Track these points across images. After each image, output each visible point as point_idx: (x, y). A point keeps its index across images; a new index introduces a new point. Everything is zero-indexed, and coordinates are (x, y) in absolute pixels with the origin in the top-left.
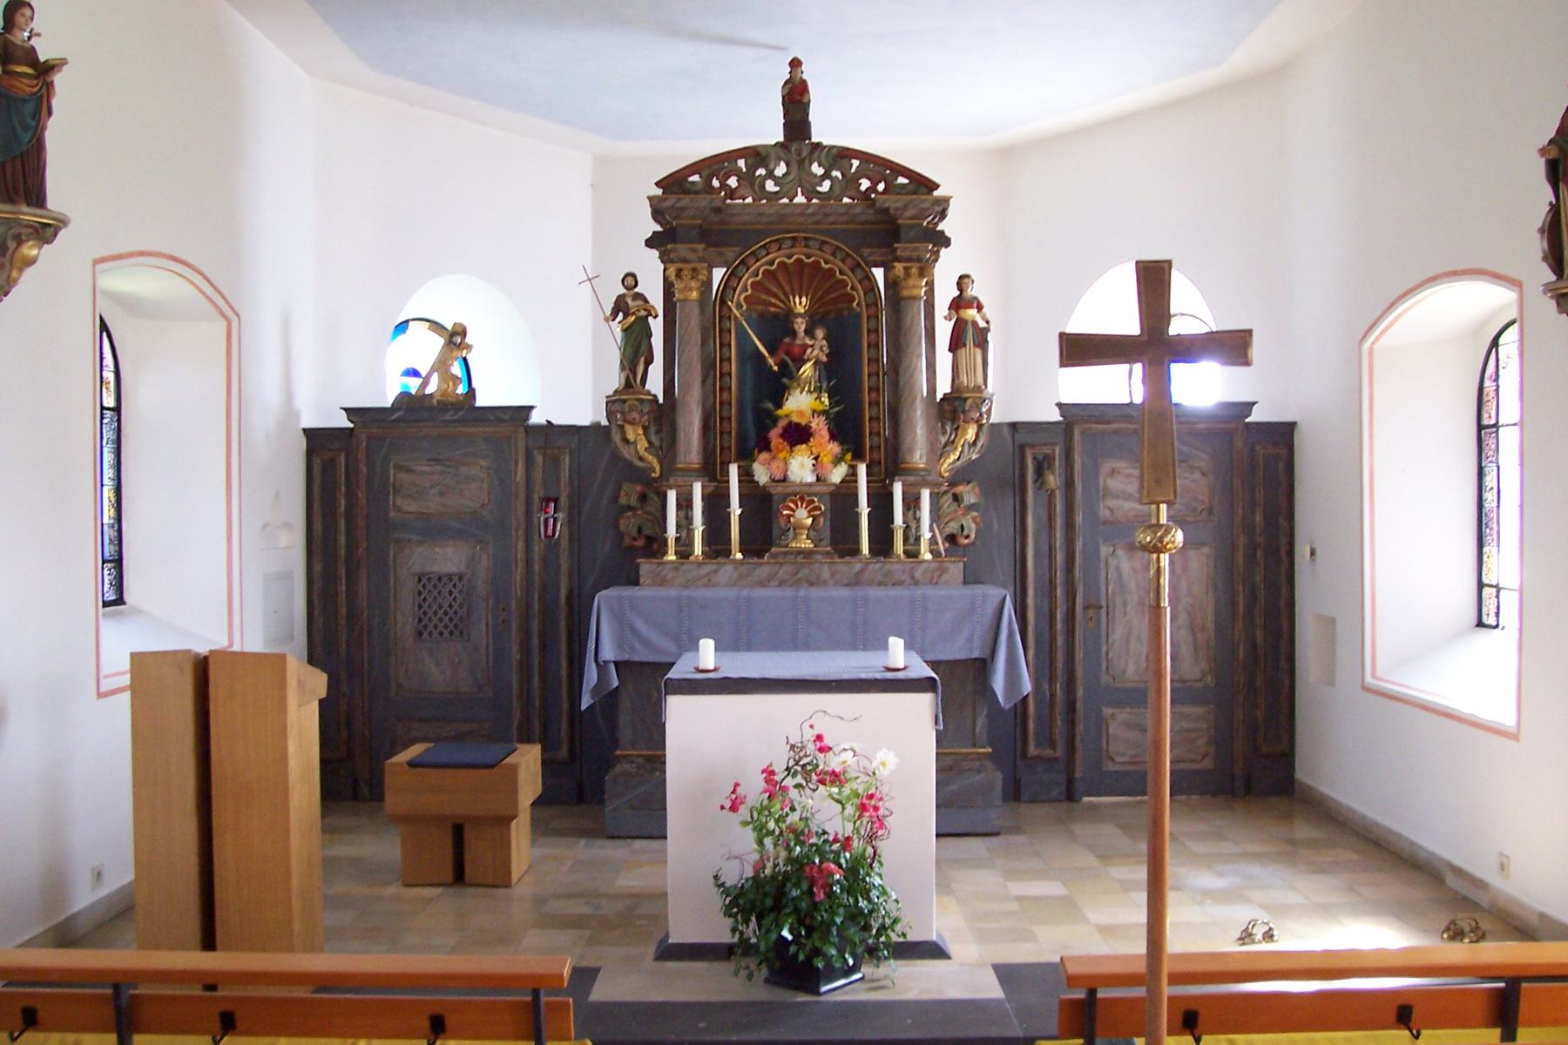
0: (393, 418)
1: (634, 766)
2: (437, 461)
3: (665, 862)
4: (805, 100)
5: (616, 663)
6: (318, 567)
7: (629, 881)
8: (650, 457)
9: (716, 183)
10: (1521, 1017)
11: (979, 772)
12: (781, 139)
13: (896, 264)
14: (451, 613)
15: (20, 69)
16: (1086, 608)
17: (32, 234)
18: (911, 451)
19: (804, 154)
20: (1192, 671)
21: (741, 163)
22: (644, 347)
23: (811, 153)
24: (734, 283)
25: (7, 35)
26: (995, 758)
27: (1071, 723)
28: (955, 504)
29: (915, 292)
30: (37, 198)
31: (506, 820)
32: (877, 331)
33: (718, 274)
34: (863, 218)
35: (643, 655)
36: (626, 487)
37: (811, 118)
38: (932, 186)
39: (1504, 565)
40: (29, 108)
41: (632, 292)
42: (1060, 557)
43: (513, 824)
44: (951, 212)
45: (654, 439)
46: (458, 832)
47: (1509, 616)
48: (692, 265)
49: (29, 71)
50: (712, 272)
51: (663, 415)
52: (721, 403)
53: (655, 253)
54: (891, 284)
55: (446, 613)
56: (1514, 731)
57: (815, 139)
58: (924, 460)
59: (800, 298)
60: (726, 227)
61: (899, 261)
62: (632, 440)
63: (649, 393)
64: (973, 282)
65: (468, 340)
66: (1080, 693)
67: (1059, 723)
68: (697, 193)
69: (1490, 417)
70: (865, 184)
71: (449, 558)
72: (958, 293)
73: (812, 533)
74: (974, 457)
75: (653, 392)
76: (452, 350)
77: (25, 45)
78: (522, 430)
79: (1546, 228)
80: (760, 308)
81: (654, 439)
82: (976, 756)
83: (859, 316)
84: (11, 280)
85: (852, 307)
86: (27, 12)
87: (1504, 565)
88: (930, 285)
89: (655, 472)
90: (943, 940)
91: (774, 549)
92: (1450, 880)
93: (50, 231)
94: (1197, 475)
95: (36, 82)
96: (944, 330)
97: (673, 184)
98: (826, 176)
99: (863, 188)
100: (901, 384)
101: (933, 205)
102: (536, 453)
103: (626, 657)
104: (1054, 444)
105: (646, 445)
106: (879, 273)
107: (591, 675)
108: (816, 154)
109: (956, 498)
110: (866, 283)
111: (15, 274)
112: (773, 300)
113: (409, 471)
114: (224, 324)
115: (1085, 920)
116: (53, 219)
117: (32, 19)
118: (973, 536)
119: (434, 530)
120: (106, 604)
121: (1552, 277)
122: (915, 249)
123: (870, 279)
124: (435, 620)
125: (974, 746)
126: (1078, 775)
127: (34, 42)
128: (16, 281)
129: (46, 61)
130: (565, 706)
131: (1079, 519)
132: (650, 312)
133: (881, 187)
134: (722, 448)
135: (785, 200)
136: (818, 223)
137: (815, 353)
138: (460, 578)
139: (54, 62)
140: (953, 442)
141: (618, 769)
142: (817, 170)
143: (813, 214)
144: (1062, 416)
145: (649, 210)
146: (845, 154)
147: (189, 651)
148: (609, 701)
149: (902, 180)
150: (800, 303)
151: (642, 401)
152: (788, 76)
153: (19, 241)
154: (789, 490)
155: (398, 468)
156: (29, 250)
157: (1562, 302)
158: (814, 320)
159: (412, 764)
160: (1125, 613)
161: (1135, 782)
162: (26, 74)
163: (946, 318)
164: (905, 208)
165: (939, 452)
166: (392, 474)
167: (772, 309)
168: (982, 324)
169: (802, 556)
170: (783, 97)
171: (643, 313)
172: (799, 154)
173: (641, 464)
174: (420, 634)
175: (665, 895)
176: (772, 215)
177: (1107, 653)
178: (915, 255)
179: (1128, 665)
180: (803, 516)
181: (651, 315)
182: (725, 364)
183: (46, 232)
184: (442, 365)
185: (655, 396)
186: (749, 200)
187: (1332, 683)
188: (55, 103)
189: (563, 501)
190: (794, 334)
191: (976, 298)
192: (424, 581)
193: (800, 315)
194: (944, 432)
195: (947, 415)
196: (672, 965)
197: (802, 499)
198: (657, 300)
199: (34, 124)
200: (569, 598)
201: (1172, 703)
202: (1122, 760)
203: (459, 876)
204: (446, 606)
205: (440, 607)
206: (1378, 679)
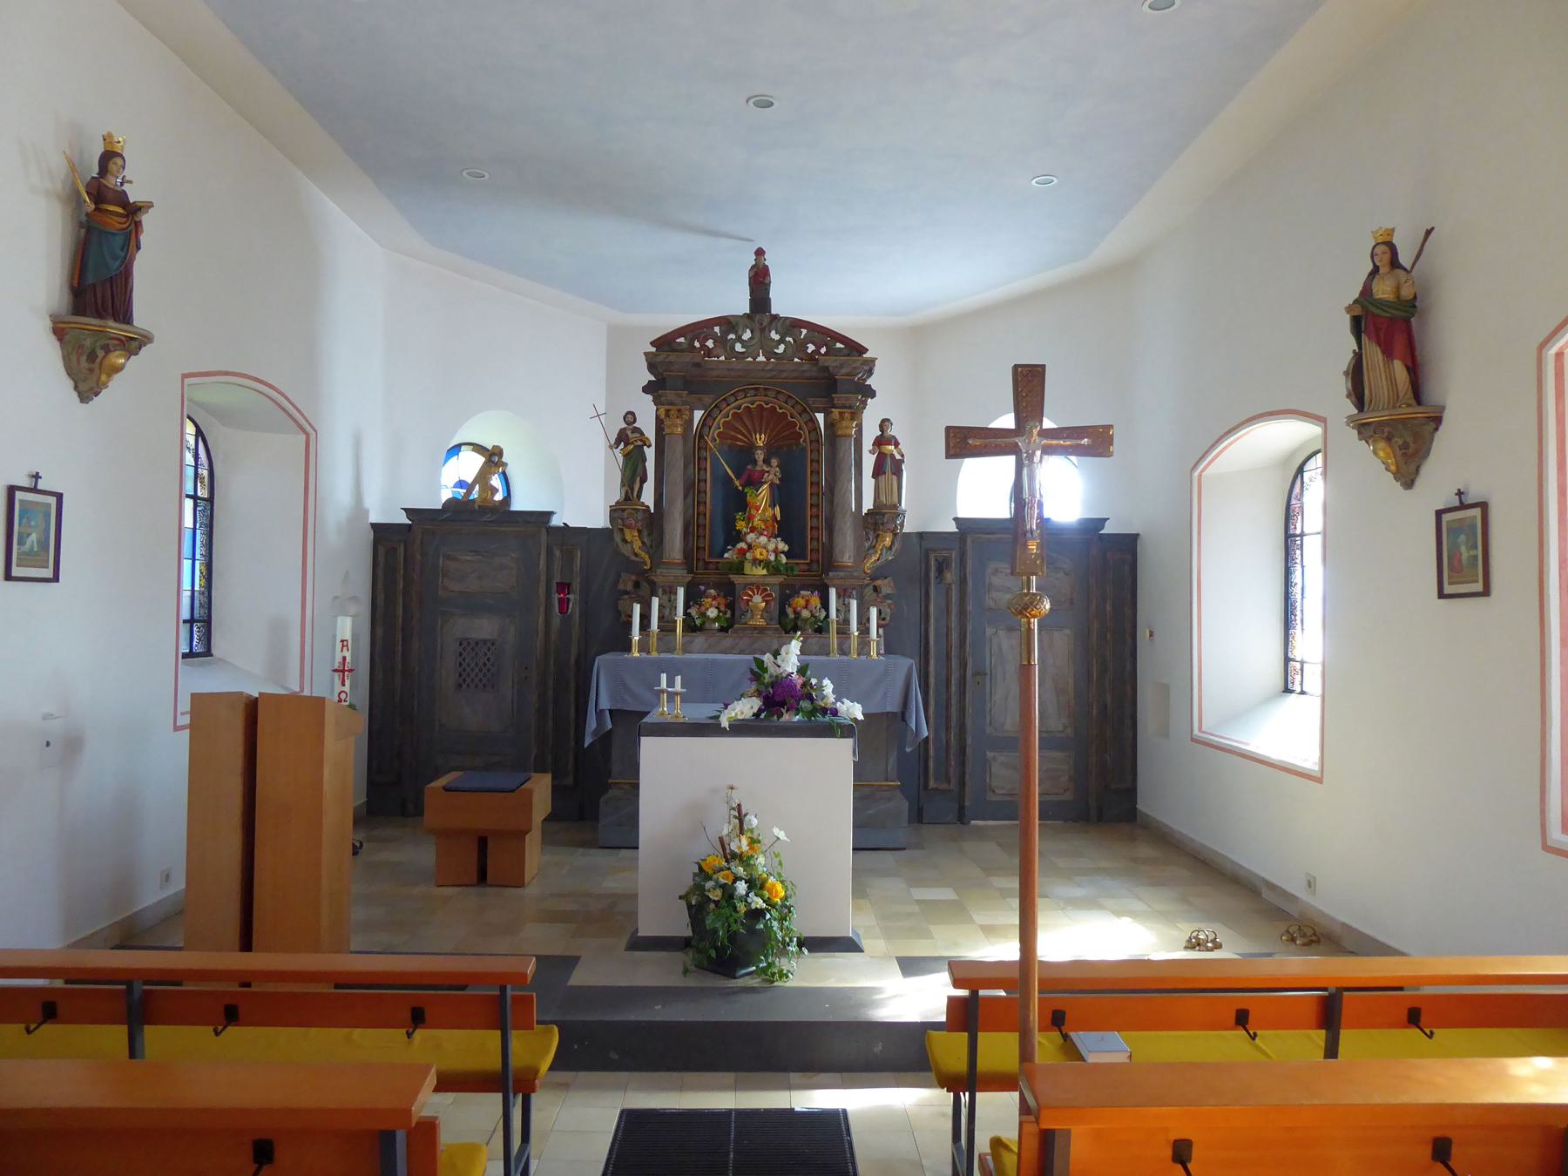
0: (441, 518)
1: (622, 791)
2: (476, 552)
3: (636, 868)
4: (767, 282)
5: (610, 711)
6: (380, 632)
7: (612, 884)
8: (643, 553)
9: (697, 344)
10: (1343, 1021)
11: (890, 800)
13: (833, 410)
14: (484, 670)
15: (112, 208)
16: (975, 675)
17: (118, 345)
18: (843, 553)
19: (765, 324)
20: (1058, 724)
21: (717, 329)
22: (639, 470)
23: (771, 322)
24: (709, 422)
25: (101, 180)
26: (902, 789)
27: (963, 764)
28: (875, 594)
29: (848, 431)
30: (125, 316)
31: (521, 834)
32: (818, 461)
33: (698, 415)
34: (808, 374)
35: (632, 706)
36: (624, 576)
37: (771, 296)
38: (861, 350)
39: (1310, 644)
40: (119, 241)
41: (631, 427)
42: (955, 636)
43: (527, 837)
44: (876, 370)
46: (483, 842)
47: (1313, 680)
48: (678, 407)
49: (120, 210)
50: (693, 413)
51: (654, 523)
52: (698, 514)
53: (650, 397)
54: (830, 425)
55: (481, 671)
56: (1319, 776)
57: (773, 312)
58: (852, 560)
59: (760, 435)
60: (704, 379)
61: (836, 408)
62: (629, 541)
63: (643, 504)
64: (892, 424)
65: (504, 460)
66: (969, 741)
67: (953, 763)
68: (682, 351)
69: (1295, 528)
70: (811, 348)
71: (484, 628)
73: (765, 615)
74: (890, 558)
75: (646, 504)
76: (491, 467)
77: (118, 189)
78: (544, 531)
79: (1350, 372)
80: (729, 441)
81: (646, 540)
82: (886, 788)
83: (804, 449)
84: (100, 382)
85: (799, 443)
86: (119, 161)
87: (1310, 644)
88: (860, 427)
89: (646, 565)
90: (858, 935)
91: (736, 626)
92: (1266, 894)
93: (134, 344)
94: (1061, 575)
95: (125, 220)
97: (664, 343)
98: (782, 341)
99: (809, 351)
100: (835, 502)
101: (862, 365)
102: (554, 548)
103: (619, 706)
104: (952, 549)
105: (640, 544)
106: (820, 417)
107: (592, 724)
108: (774, 324)
109: (876, 589)
110: (810, 424)
111: (104, 378)
112: (740, 437)
113: (455, 559)
114: (303, 437)
115: (974, 923)
116: (139, 335)
117: (124, 168)
118: (888, 618)
119: (474, 605)
122: (847, 399)
123: (814, 421)
124: (473, 675)
125: (887, 780)
126: (967, 803)
127: (126, 187)
128: (105, 385)
129: (134, 203)
130: (572, 744)
131: (970, 607)
132: (645, 443)
133: (823, 350)
134: (698, 548)
135: (750, 359)
136: (773, 377)
137: (771, 477)
138: (493, 644)
139: (141, 204)
140: (874, 547)
141: (611, 793)
142: (775, 336)
143: (771, 370)
144: (957, 528)
145: (645, 364)
146: (797, 324)
147: (242, 693)
148: (605, 739)
149: (839, 345)
150: (760, 439)
151: (637, 510)
152: (754, 263)
153: (107, 350)
154: (749, 581)
155: (447, 557)
157: (1363, 430)
158: (771, 450)
159: (446, 789)
160: (1004, 679)
161: (1011, 809)
162: (117, 212)
163: (870, 452)
164: (841, 366)
165: (862, 555)
166: (441, 562)
168: (898, 457)
169: (757, 631)
170: (750, 278)
171: (640, 443)
172: (761, 324)
173: (633, 558)
174: (460, 686)
175: (636, 895)
176: (739, 370)
177: (991, 710)
178: (847, 403)
179: (1009, 721)
180: (757, 599)
181: (646, 445)
182: (702, 484)
183: (133, 344)
184: (483, 477)
185: (648, 507)
186: (722, 358)
187: (1166, 735)
188: (143, 239)
189: (576, 586)
190: (755, 462)
191: (894, 437)
192: (465, 644)
195: (870, 526)
196: (638, 954)
197: (758, 588)
198: (650, 433)
199: (123, 254)
200: (577, 661)
201: (1039, 749)
202: (1002, 792)
203: (482, 878)
204: (481, 665)
205: (477, 665)
206: (1204, 732)
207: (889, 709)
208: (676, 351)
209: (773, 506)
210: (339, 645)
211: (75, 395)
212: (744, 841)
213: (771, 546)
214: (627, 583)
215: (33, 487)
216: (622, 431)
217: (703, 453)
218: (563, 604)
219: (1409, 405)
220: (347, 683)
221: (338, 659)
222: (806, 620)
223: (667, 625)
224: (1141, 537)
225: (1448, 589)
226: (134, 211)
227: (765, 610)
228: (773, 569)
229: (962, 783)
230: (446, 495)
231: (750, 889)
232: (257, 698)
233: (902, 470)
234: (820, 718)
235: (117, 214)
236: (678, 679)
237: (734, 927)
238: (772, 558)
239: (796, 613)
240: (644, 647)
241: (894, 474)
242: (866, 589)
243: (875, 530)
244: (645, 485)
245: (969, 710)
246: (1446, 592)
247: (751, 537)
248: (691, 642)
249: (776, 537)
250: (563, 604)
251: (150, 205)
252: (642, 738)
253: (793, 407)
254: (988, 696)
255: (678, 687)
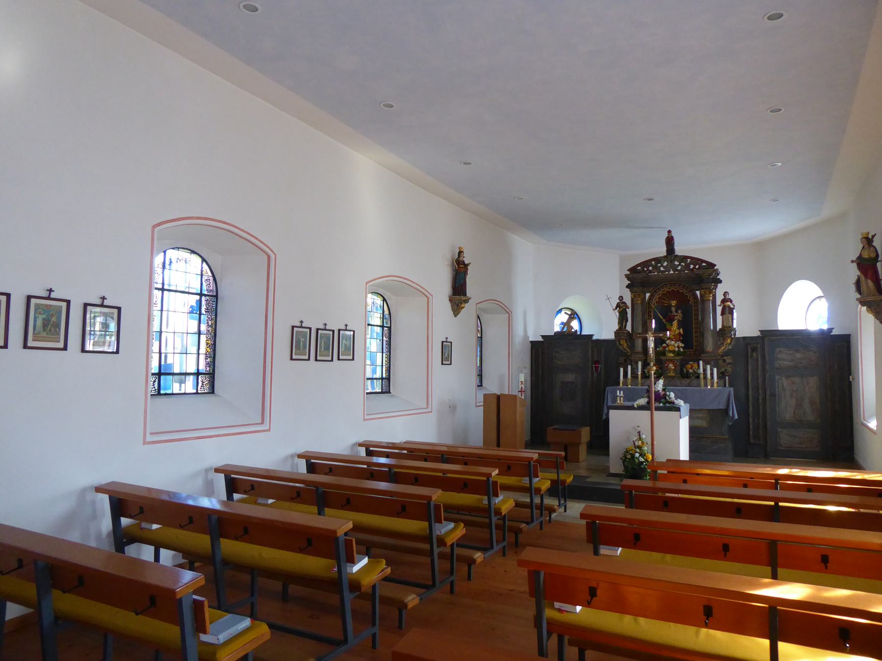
9: (645, 269)
12: (665, 254)
15: (461, 266)
18: (707, 347)
21: (653, 263)
23: (675, 258)
29: (708, 298)
30: (465, 294)
33: (648, 295)
45: (629, 344)
53: (628, 290)
63: (627, 330)
70: (692, 266)
71: (570, 377)
72: (724, 297)
74: (730, 348)
78: (590, 341)
81: (629, 344)
96: (719, 310)
97: (633, 270)
106: (698, 293)
109: (724, 361)
120: (478, 386)
121: (859, 296)
131: (767, 367)
132: (627, 307)
133: (697, 267)
135: (667, 273)
142: (677, 263)
146: (685, 258)
147: (496, 394)
149: (704, 264)
154: (668, 358)
155: (556, 352)
156: (463, 305)
158: (678, 308)
159: (554, 429)
165: (717, 346)
167: (665, 304)
168: (732, 307)
173: (624, 351)
180: (671, 366)
183: (466, 301)
186: (656, 273)
190: (672, 312)
191: (730, 299)
193: (673, 306)
194: (720, 341)
197: (671, 361)
198: (629, 303)
207: (721, 408)
208: (637, 273)
209: (679, 329)
210: (520, 383)
211: (453, 316)
212: (640, 442)
213: (676, 345)
214: (622, 359)
215: (382, 325)
216: (618, 303)
217: (650, 310)
218: (597, 368)
219: (873, 295)
220: (523, 395)
221: (520, 388)
222: (692, 373)
223: (634, 375)
224: (852, 335)
225: (294, 357)
226: (466, 266)
227: (674, 369)
228: (678, 354)
229: (766, 442)
230: (557, 328)
231: (640, 456)
232: (500, 396)
233: (733, 312)
234: (668, 405)
235: (462, 267)
236: (622, 392)
237: (634, 467)
238: (677, 349)
239: (688, 371)
240: (625, 384)
241: (730, 314)
242: (711, 361)
243: (723, 337)
244: (628, 323)
245: (768, 410)
246: (293, 358)
247: (668, 342)
248: (645, 382)
249: (678, 341)
250: (597, 368)
251: (470, 263)
252: (610, 410)
253: (686, 289)
254: (777, 404)
255: (622, 395)
